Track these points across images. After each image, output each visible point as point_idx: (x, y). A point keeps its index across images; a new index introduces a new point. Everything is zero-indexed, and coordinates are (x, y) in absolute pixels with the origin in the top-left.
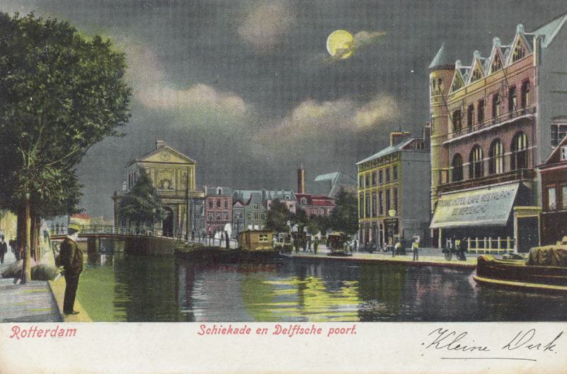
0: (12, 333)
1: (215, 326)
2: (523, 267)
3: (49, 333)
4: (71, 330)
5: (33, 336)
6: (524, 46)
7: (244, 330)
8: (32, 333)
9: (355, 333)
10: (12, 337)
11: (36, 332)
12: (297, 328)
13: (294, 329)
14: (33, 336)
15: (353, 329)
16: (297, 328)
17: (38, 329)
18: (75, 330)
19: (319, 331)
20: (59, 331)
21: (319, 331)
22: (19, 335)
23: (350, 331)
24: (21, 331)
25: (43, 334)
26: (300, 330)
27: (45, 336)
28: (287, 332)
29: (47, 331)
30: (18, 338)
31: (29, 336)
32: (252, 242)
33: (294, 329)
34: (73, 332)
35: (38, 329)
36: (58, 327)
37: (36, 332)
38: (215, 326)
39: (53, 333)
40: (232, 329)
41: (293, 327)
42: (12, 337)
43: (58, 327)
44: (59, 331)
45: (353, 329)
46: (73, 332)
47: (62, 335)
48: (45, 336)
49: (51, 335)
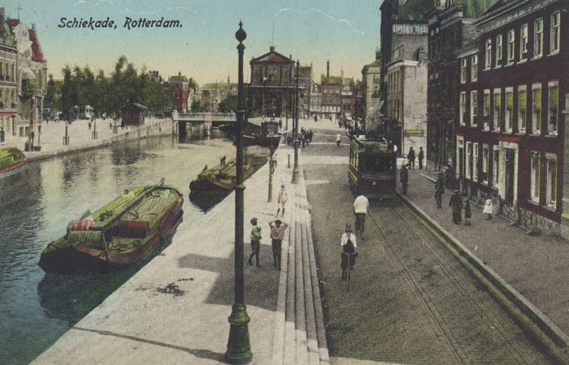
3: (155, 24)
4: (175, 22)
7: (161, 22)
9: (181, 26)
25: (150, 25)
30: (93, 29)
31: (139, 26)
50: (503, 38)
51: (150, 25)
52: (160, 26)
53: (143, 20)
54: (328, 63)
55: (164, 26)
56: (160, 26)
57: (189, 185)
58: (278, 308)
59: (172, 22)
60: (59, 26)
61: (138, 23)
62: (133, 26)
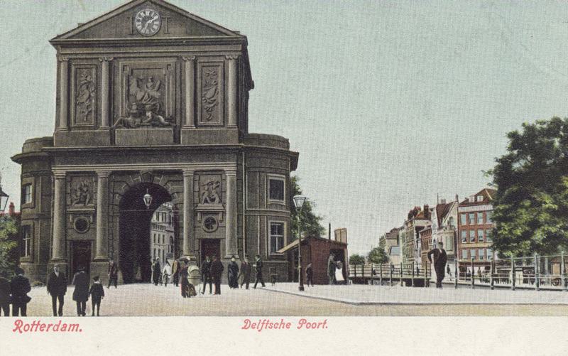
0: (244, 324)
1: (282, 320)
2: (75, 290)
3: (51, 328)
4: (74, 325)
5: (36, 330)
6: (270, 235)
7: (58, 326)
8: (35, 327)
9: (81, 330)
10: (14, 330)
11: (39, 327)
12: (266, 322)
13: (263, 324)
14: (36, 330)
15: (325, 323)
16: (266, 322)
17: (41, 323)
18: (78, 325)
19: (288, 325)
20: (61, 326)
21: (288, 325)
22: (22, 329)
23: (321, 326)
24: (23, 326)
25: (45, 329)
26: (269, 325)
27: (47, 330)
28: (256, 326)
29: (50, 326)
30: (21, 332)
31: (31, 330)
32: (341, 269)
33: (263, 324)
34: (76, 327)
35: (41, 323)
36: (60, 321)
37: (39, 327)
38: (282, 320)
39: (56, 328)
40: (284, 324)
41: (262, 322)
42: (14, 330)
43: (60, 321)
44: (61, 326)
45: (325, 323)
46: (76, 327)
47: (65, 330)
48: (47, 330)
49: (54, 330)
50: (13, 307)
51: (45, 329)
52: (57, 330)
53: (36, 323)
54: (330, 225)
55: (62, 330)
56: (57, 330)
57: (255, 86)
58: (343, 241)
59: (71, 325)
60: (299, 328)
61: (31, 327)
62: (26, 331)
